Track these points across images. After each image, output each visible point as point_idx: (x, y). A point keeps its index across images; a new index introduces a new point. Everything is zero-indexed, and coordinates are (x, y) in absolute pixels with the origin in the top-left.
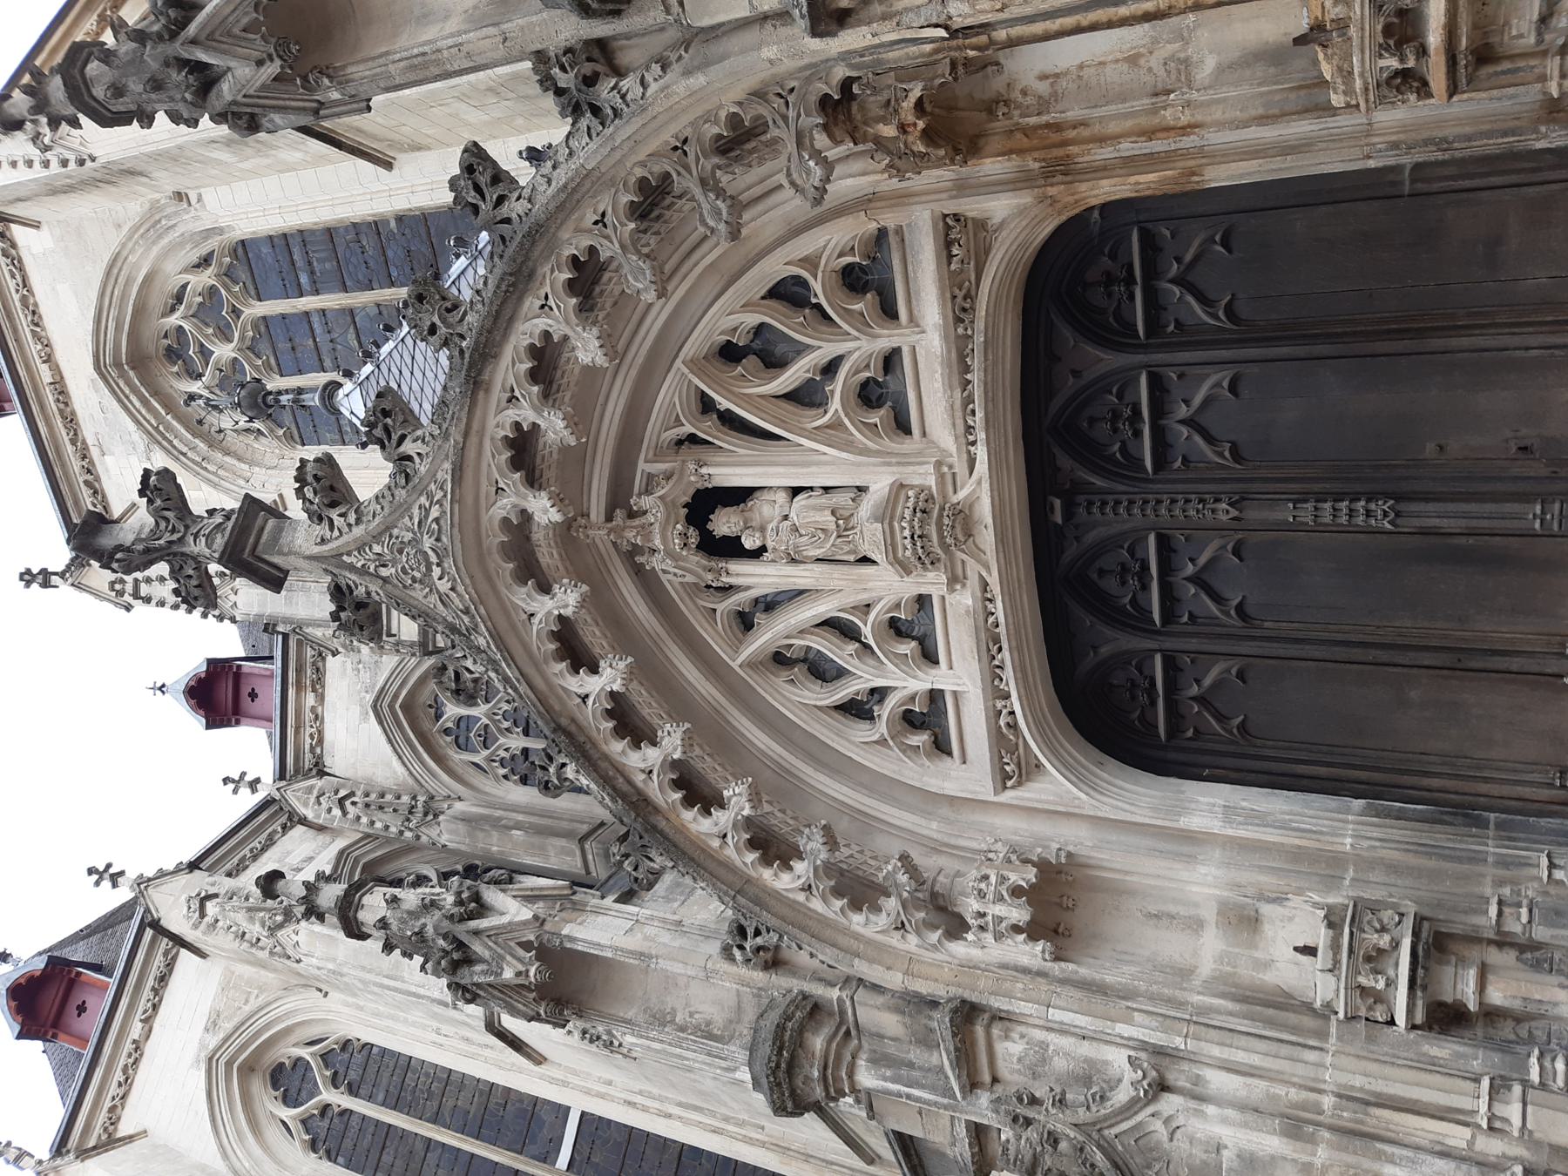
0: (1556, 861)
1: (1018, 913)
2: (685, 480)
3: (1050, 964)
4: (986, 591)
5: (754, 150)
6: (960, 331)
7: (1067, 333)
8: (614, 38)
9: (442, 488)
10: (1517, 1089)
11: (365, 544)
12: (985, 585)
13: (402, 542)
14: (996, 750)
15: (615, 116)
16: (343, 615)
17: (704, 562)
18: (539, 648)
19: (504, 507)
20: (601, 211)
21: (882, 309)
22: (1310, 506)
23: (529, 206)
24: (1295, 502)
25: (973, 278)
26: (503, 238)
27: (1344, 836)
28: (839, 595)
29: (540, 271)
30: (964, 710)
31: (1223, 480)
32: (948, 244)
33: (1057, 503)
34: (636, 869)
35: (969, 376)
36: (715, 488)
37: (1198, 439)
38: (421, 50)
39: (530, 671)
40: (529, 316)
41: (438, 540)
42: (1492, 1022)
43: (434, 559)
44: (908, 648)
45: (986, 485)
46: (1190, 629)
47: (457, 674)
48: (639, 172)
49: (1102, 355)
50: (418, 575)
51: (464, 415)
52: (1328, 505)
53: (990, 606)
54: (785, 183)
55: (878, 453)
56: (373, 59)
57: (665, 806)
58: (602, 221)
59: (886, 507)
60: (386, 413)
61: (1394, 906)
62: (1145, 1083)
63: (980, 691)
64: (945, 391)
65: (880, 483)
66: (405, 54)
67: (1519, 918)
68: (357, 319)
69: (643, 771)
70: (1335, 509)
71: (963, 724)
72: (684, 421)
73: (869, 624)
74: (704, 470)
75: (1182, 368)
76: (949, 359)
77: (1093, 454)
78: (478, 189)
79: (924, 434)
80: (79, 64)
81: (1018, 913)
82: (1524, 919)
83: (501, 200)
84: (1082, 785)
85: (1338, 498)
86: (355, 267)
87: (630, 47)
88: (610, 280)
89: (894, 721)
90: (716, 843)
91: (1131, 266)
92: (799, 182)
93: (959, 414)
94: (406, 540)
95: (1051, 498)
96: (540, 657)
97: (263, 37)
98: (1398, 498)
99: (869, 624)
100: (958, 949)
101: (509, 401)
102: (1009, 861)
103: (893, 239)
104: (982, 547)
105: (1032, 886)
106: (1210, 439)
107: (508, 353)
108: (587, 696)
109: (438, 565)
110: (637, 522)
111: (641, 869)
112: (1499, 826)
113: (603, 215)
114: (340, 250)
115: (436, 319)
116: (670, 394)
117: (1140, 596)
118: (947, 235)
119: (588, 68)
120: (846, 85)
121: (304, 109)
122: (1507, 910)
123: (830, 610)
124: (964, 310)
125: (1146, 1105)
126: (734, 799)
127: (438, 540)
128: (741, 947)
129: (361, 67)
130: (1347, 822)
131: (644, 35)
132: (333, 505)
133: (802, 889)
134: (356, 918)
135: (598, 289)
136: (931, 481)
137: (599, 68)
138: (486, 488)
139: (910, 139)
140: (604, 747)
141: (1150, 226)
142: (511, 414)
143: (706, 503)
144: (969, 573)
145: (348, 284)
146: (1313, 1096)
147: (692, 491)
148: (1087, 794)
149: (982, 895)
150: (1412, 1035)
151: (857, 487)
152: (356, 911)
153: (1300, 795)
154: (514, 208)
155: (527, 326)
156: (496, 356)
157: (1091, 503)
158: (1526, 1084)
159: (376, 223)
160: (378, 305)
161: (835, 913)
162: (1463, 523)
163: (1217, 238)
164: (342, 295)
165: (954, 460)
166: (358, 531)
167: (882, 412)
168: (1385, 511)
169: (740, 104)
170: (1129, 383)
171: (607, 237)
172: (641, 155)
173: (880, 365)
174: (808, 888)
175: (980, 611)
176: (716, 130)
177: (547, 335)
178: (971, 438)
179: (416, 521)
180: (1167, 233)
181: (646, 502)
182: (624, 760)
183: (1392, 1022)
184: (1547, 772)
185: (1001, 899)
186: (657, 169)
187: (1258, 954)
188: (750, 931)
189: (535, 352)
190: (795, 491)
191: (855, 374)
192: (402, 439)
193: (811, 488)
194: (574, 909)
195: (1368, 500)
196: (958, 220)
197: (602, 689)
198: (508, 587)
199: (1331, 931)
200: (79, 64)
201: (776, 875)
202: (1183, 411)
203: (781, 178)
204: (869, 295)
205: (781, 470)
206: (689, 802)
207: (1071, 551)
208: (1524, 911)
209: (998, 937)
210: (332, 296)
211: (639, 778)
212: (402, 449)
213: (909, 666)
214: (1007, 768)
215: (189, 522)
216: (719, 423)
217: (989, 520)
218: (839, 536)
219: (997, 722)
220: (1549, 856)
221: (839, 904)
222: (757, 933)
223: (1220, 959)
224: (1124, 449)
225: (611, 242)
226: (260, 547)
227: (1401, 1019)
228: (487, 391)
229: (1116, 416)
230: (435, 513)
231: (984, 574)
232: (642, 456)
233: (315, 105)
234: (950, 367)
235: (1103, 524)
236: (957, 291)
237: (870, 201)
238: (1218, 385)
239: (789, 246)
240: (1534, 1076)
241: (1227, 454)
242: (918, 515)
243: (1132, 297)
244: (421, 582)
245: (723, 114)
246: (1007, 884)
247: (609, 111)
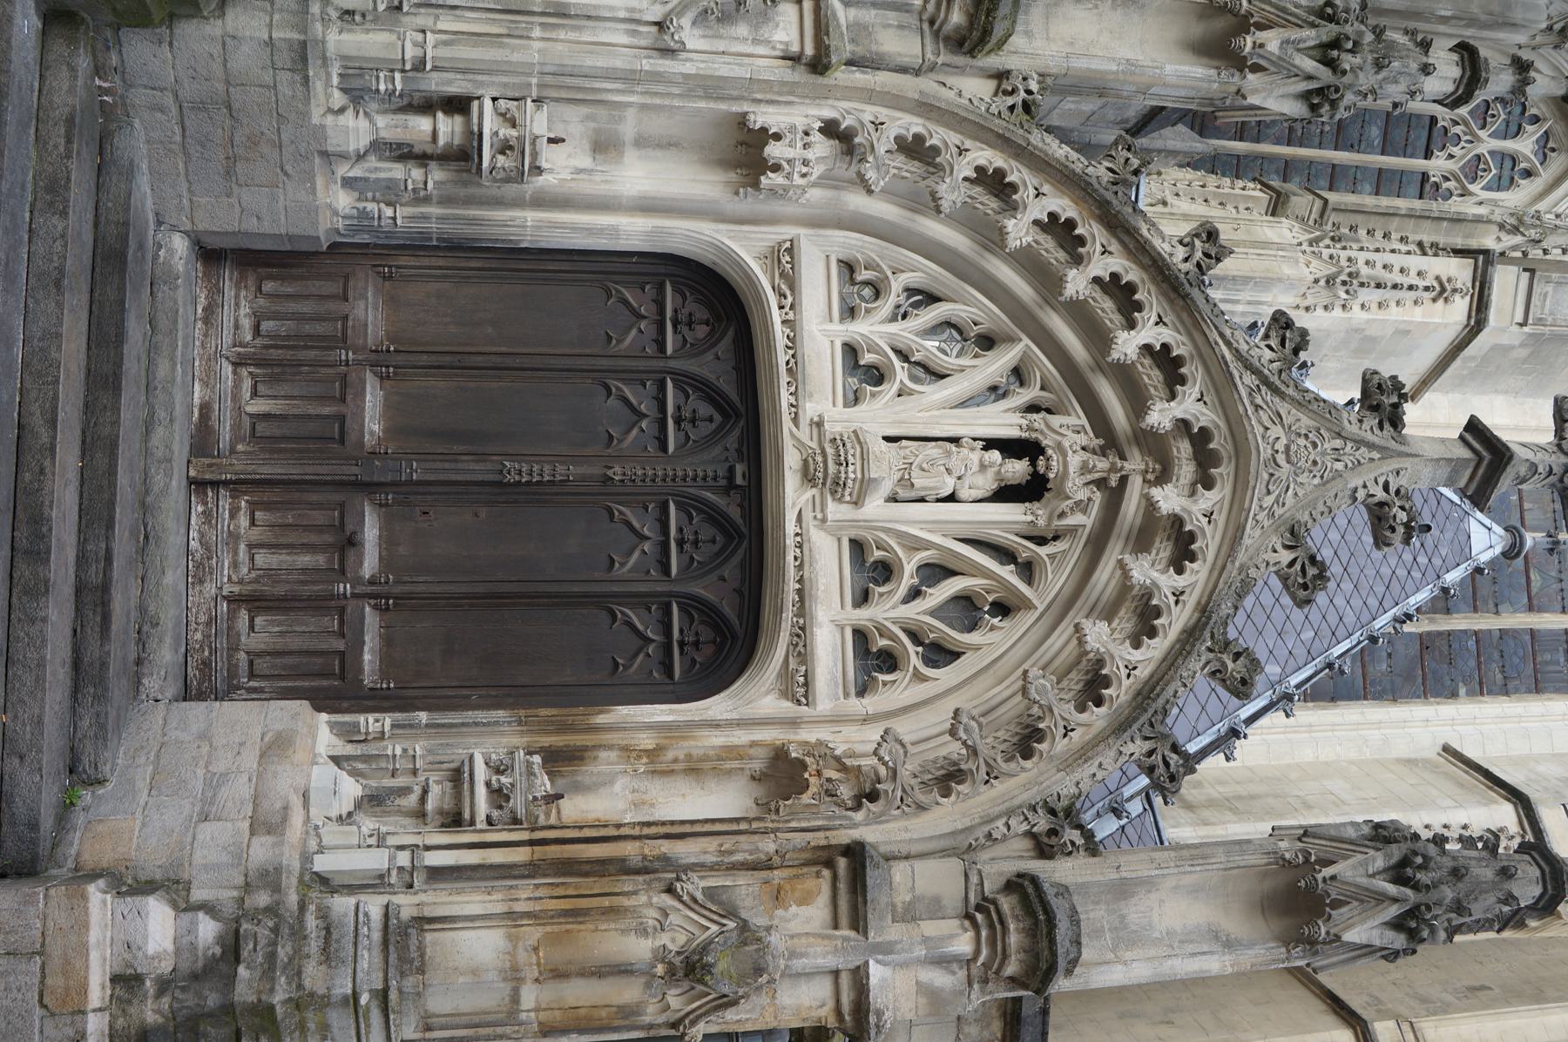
1: (774, 151)
2: (1048, 511)
4: (796, 414)
7: (729, 611)
8: (1033, 858)
10: (408, 67)
11: (1352, 469)
13: (1311, 472)
16: (1395, 399)
24: (568, 481)
25: (791, 657)
26: (1152, 725)
29: (1129, 697)
30: (823, 306)
31: (619, 494)
32: (806, 684)
33: (739, 481)
34: (1128, 159)
35: (797, 586)
37: (637, 525)
38: (1193, 869)
39: (1205, 349)
41: (1272, 475)
43: (1281, 458)
44: (867, 358)
45: (788, 502)
46: (644, 376)
47: (1283, 344)
48: (1028, 764)
49: (702, 592)
50: (1302, 442)
51: (1221, 585)
52: (547, 478)
54: (909, 747)
55: (876, 529)
56: (1238, 867)
57: (1092, 222)
60: (1305, 587)
61: (495, 180)
62: (672, 29)
63: (806, 328)
65: (875, 508)
68: (1526, 600)
71: (826, 293)
72: (1046, 559)
74: (1030, 518)
77: (715, 517)
78: (1167, 764)
80: (1547, 897)
81: (774, 151)
82: (410, 181)
83: (1150, 753)
85: (539, 483)
86: (1515, 653)
88: (1077, 683)
90: (1046, 188)
91: (681, 653)
92: (899, 747)
93: (806, 559)
94: (1306, 474)
96: (1197, 362)
97: (1329, 896)
98: (499, 484)
100: (829, 113)
101: (1182, 593)
103: (853, 691)
105: (764, 173)
106: (629, 524)
107: (1173, 634)
109: (1277, 452)
111: (1122, 161)
113: (1065, 735)
114: (1529, 670)
115: (1230, 665)
116: (1056, 581)
117: (682, 401)
119: (1053, 841)
120: (858, 807)
121: (1314, 837)
122: (422, 186)
123: (933, 393)
124: (798, 636)
125: (671, 11)
126: (1022, 234)
127: (1272, 475)
129: (1252, 862)
132: (1381, 504)
134: (1464, 69)
135: (1089, 677)
137: (1046, 840)
138: (1221, 519)
139: (815, 767)
140: (1145, 277)
141: (667, 681)
142: (1180, 582)
143: (1032, 490)
144: (807, 430)
145: (1528, 637)
146: (547, 35)
150: (480, 93)
152: (1462, 77)
156: (1184, 631)
157: (715, 479)
159: (1482, 694)
160: (1497, 613)
162: (461, 466)
164: (1537, 627)
166: (1357, 482)
169: (937, 803)
170: (686, 568)
172: (1023, 777)
173: (870, 596)
174: (962, 151)
176: (960, 788)
177: (1137, 645)
178: (798, 539)
179: (1290, 492)
180: (655, 674)
182: (1127, 263)
183: (494, 99)
185: (789, 161)
186: (1013, 765)
187: (593, 125)
188: (1019, 109)
189: (1152, 633)
190: (952, 498)
192: (1292, 564)
193: (938, 500)
198: (1218, 427)
200: (1547, 897)
203: (912, 750)
204: (875, 650)
205: (959, 518)
206: (1070, 224)
207: (732, 440)
209: (792, 129)
210: (1549, 627)
211: (1114, 246)
212: (1292, 556)
215: (1559, 485)
217: (787, 473)
221: (934, 141)
222: (1012, 108)
223: (621, 119)
224: (691, 518)
226: (1473, 464)
227: (488, 103)
228: (1199, 603)
230: (1269, 501)
233: (1304, 839)
234: (811, 595)
235: (708, 463)
238: (623, 565)
240: (398, 76)
241: (616, 513)
243: (681, 631)
244: (1299, 435)
245: (953, 797)
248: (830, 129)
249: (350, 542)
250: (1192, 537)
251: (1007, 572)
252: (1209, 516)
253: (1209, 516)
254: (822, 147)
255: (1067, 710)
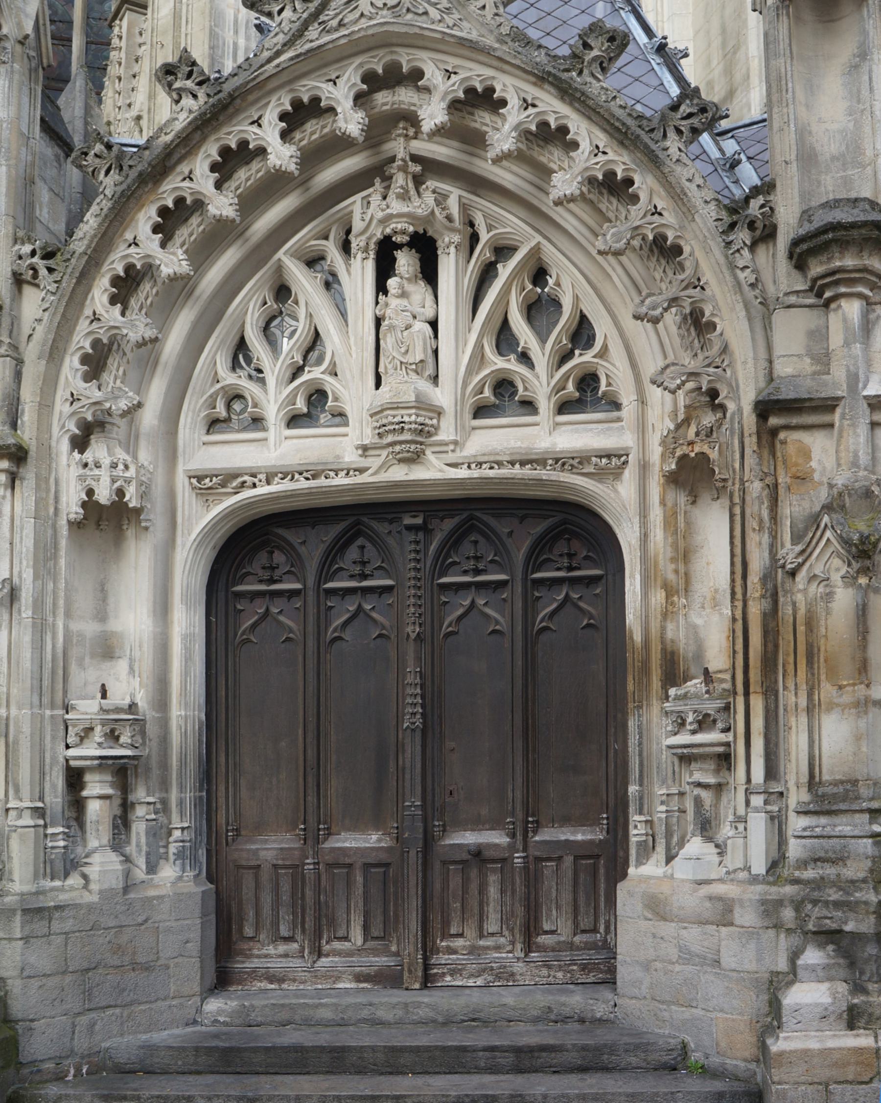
0: (185, 832)
1: (104, 495)
3: (65, 518)
4: (355, 470)
5: (689, 334)
6: (550, 462)
8: (775, 245)
9: (455, 25)
10: (41, 822)
12: (361, 471)
14: (223, 472)
15: (727, 243)
17: (374, 240)
18: (304, 86)
19: (433, 75)
20: (664, 213)
21: (567, 402)
22: (418, 680)
23: (674, 160)
25: (584, 471)
27: (186, 710)
28: (347, 353)
29: (625, 153)
30: (251, 447)
32: (608, 456)
33: (419, 521)
34: (96, 155)
36: (436, 256)
37: (460, 611)
38: (790, 90)
40: (592, 135)
42: (73, 805)
44: (301, 405)
45: (438, 475)
48: (687, 249)
49: (522, 551)
51: (517, 62)
52: (418, 691)
53: (343, 473)
54: (667, 362)
58: (656, 212)
59: (427, 404)
63: (273, 463)
64: (509, 449)
66: (789, 73)
67: (147, 814)
69: (191, 172)
70: (416, 695)
72: (492, 233)
73: (322, 376)
74: (452, 250)
75: (510, 601)
76: (531, 454)
77: (453, 541)
79: (474, 429)
81: (104, 495)
82: (148, 817)
83: (679, 132)
84: (201, 536)
85: (423, 697)
87: (768, 253)
88: (611, 203)
89: (236, 389)
91: (579, 569)
92: (668, 371)
93: (492, 458)
95: (422, 516)
96: (297, 85)
98: (424, 732)
99: (322, 376)
100: (65, 445)
102: (141, 485)
103: (615, 414)
104: (390, 469)
105: (126, 504)
107: (563, 109)
108: (260, 126)
110: (411, 185)
111: (97, 160)
112: (201, 798)
113: (660, 214)
118: (615, 456)
119: (759, 225)
120: (722, 408)
124: (564, 464)
128: (33, 253)
130: (194, 711)
131: (773, 267)
133: (94, 313)
135: (605, 191)
136: (442, 436)
139: (685, 447)
141: (604, 581)
142: (514, 102)
147: (435, 236)
148: (195, 540)
149: (114, 466)
151: (437, 376)
153: (204, 680)
154: (673, 143)
155: (584, 133)
156: (562, 99)
157: (417, 543)
158: (45, 826)
161: (79, 342)
162: (408, 764)
163: (592, 621)
165: (458, 454)
167: (493, 398)
168: (415, 723)
171: (645, 216)
174: (96, 318)
175: (340, 467)
178: (473, 466)
180: (598, 591)
181: (429, 199)
182: (201, 155)
183: (68, 747)
184: (236, 822)
185: (113, 481)
186: (687, 264)
187: (87, 660)
188: (51, 263)
190: (434, 324)
191: (522, 379)
193: (436, 336)
194: (30, 70)
195: (422, 714)
196: (624, 464)
197: (269, 144)
198: (361, 65)
199: (127, 707)
201: (106, 290)
202: (481, 602)
207: (382, 528)
208: (153, 816)
211: (184, 168)
213: (287, 406)
214: (207, 480)
216: (487, 262)
217: (412, 477)
218: (401, 363)
219: (246, 474)
220: (188, 827)
222: (50, 270)
223: (80, 635)
224: (454, 563)
225: (642, 218)
227: (71, 752)
228: (535, 84)
229: (477, 558)
231: (370, 471)
232: (464, 194)
234: (526, 454)
236: (577, 460)
237: (643, 402)
238: (497, 622)
239: (619, 341)
240: (50, 831)
241: (450, 629)
242: (420, 427)
243: (558, 569)
246: (126, 485)
247: (731, 238)
248: (80, 443)
249: (478, 855)
250: (470, 91)
251: (505, 271)
252: (449, 74)
253: (449, 74)
254: (98, 450)
255: (636, 212)
